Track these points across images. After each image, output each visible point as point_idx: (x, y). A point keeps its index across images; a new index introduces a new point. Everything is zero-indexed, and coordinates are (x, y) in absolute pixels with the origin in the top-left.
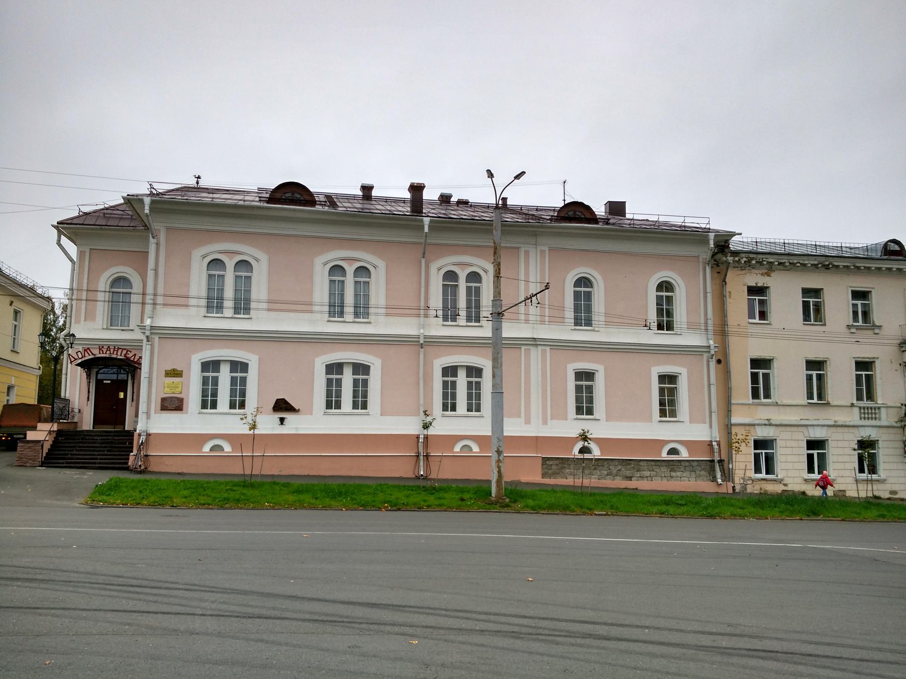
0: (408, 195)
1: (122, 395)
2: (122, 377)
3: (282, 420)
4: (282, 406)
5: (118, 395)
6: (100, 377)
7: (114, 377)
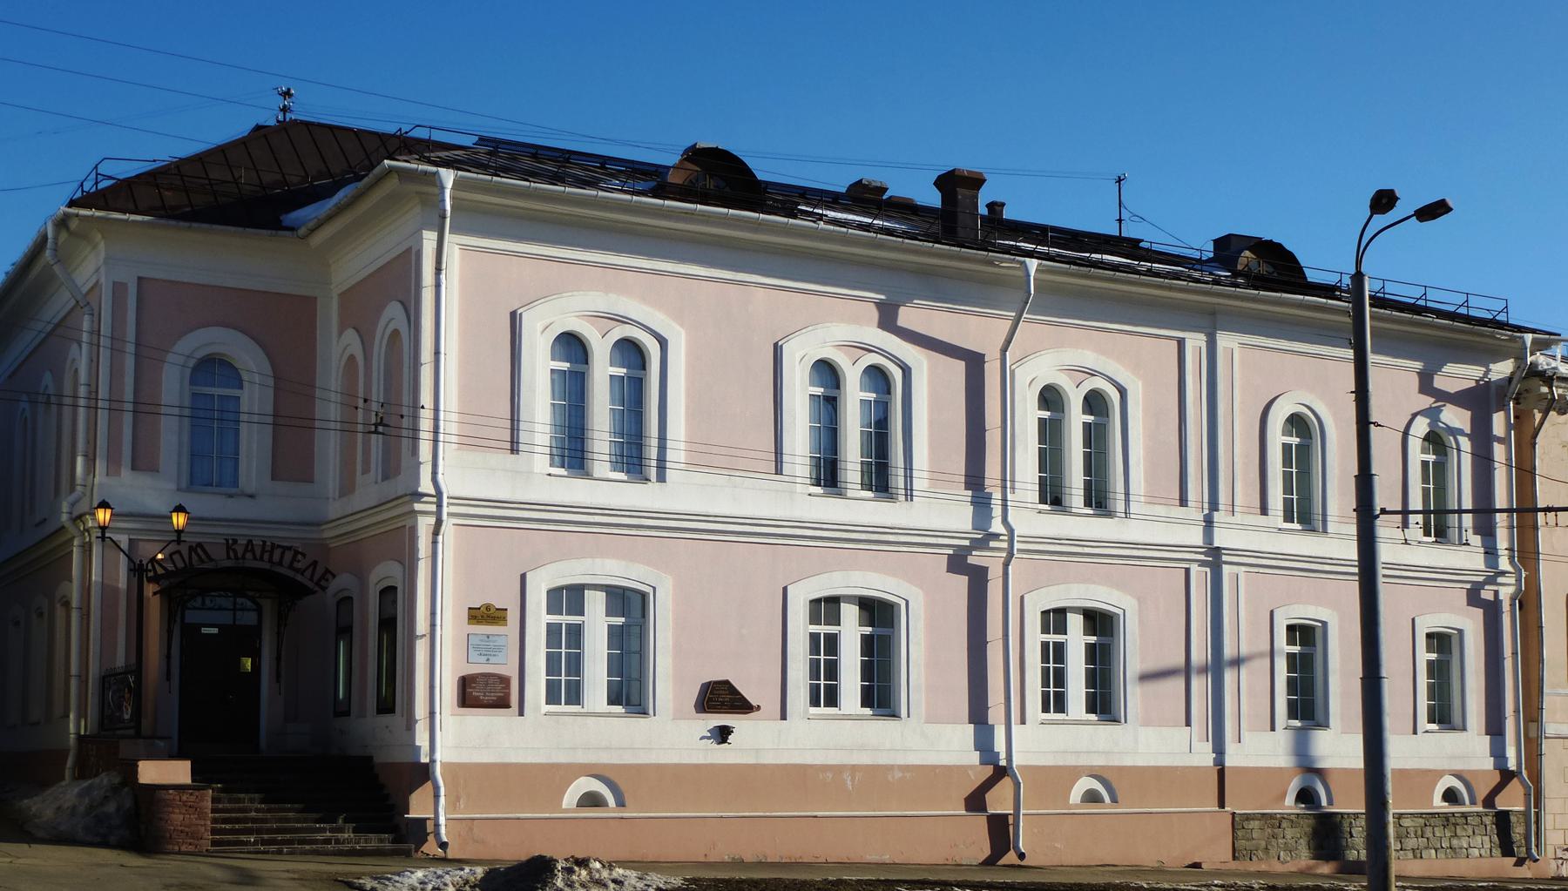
0: (933, 199)
1: (248, 663)
2: (249, 618)
3: (723, 734)
4: (720, 698)
5: (238, 663)
6: (192, 617)
7: (226, 617)
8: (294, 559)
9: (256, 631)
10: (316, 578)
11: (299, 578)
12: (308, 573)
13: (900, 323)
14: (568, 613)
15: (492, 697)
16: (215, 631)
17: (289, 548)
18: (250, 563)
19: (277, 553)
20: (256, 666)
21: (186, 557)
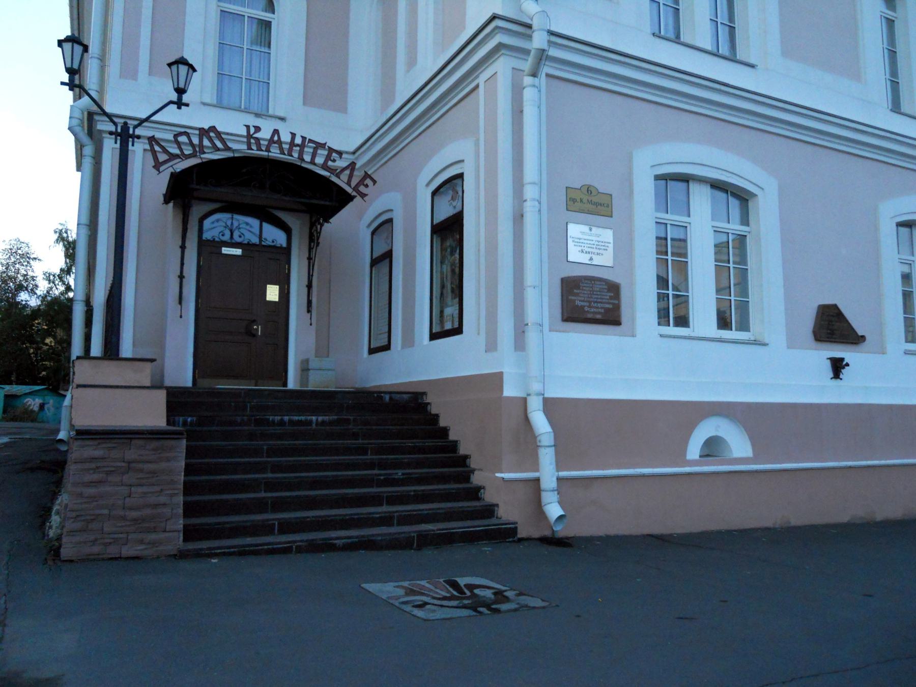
1: (273, 293)
3: (838, 366)
8: (328, 158)
9: (285, 252)
10: (353, 184)
11: (334, 179)
12: (345, 176)
13: (738, 57)
14: (265, 491)
15: (597, 310)
16: (238, 252)
17: (323, 146)
18: (275, 153)
19: (308, 150)
20: (285, 295)
21: (196, 141)
